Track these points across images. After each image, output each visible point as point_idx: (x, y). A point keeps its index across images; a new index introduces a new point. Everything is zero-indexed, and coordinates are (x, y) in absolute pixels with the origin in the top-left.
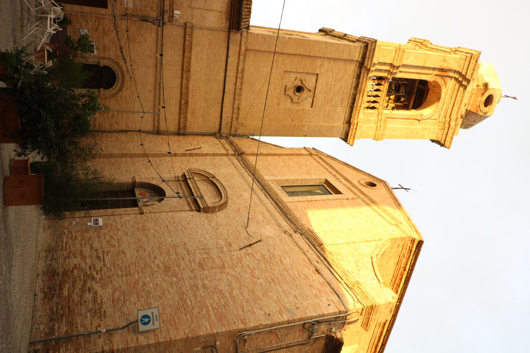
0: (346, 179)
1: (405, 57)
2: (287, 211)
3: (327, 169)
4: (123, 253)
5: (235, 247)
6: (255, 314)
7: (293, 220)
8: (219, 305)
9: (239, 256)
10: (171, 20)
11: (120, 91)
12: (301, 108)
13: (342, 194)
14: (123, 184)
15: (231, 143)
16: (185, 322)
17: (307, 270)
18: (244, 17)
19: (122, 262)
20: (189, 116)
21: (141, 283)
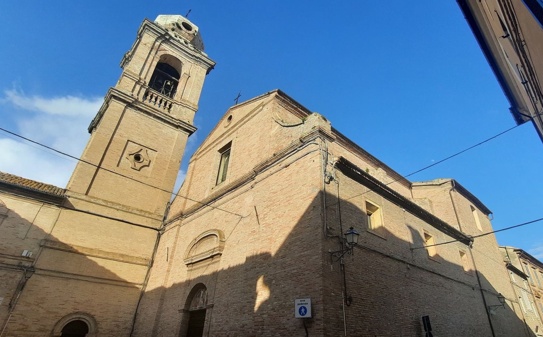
0: (221, 136)
1: (133, 71)
2: (236, 184)
3: (210, 149)
4: (243, 326)
5: (256, 227)
6: (312, 218)
7: (245, 179)
8: (300, 246)
9: (264, 225)
10: (32, 260)
11: (93, 317)
12: (155, 159)
13: (232, 141)
14: (183, 322)
15: (171, 222)
16: (310, 276)
17: (285, 174)
18: (52, 191)
19: (251, 328)
20: (137, 255)
21: (272, 313)
